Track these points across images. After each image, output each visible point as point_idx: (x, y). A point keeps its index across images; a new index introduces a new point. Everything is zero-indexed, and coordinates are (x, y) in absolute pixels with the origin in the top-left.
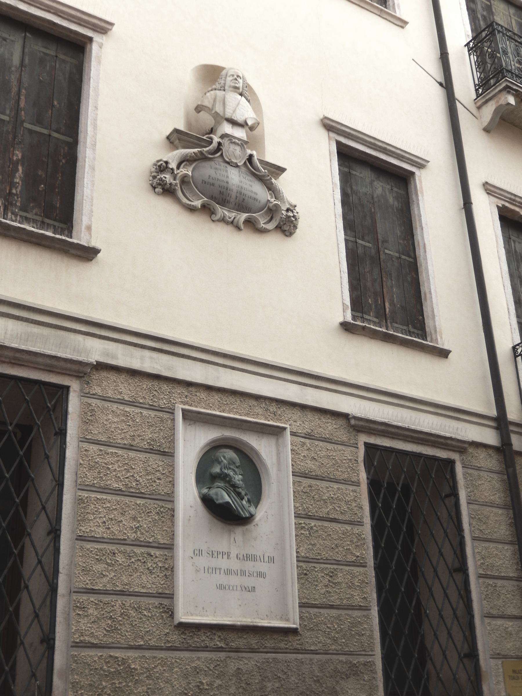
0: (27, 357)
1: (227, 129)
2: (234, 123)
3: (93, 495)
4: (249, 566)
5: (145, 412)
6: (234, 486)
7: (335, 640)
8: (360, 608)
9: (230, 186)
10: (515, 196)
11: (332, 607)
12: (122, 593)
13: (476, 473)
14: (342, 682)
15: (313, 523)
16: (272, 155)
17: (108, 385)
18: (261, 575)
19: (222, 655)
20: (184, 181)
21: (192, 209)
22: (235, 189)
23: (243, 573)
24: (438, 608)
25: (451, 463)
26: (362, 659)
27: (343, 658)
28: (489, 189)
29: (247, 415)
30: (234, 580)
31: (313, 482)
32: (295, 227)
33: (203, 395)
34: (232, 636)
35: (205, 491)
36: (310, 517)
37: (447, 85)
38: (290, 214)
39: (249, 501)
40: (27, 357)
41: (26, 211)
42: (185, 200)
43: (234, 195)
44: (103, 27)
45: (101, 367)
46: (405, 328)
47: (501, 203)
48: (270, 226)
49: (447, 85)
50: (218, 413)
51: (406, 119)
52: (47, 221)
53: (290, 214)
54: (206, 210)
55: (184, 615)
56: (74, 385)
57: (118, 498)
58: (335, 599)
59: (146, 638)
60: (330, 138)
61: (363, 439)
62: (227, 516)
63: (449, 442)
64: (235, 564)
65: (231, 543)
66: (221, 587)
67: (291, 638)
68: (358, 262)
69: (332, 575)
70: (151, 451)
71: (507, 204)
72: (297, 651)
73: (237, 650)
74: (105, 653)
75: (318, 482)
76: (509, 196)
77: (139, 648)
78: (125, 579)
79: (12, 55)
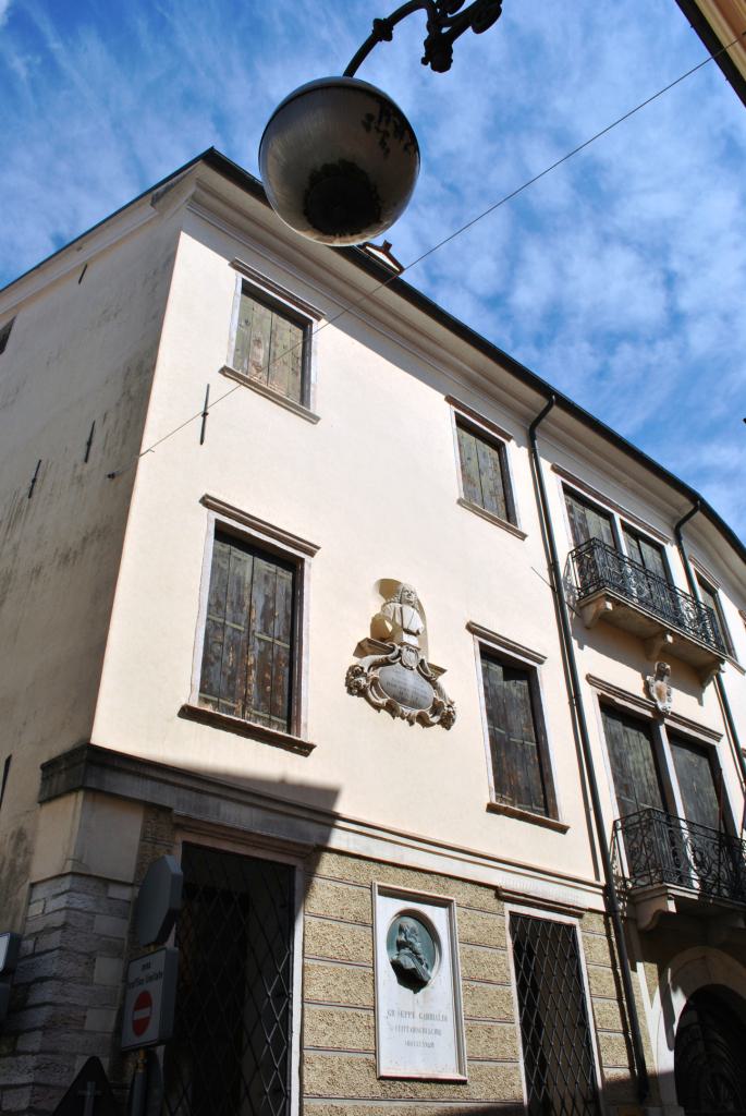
0: (265, 841)
1: (406, 638)
2: (409, 632)
3: (316, 963)
4: (429, 1024)
5: (350, 888)
6: (416, 953)
9: (408, 687)
11: (491, 1060)
12: (339, 1050)
15: (475, 984)
16: (433, 658)
18: (437, 1032)
20: (374, 682)
21: (377, 707)
22: (411, 689)
23: (424, 1031)
24: (250, 1098)
25: (292, 868)
28: (591, 679)
29: (423, 888)
30: (419, 1037)
31: (474, 948)
32: (454, 721)
33: (391, 870)
34: (418, 1086)
35: (395, 957)
38: (451, 709)
39: (427, 966)
40: (265, 841)
41: (258, 710)
42: (373, 699)
43: (410, 694)
44: (311, 550)
46: (529, 807)
50: (402, 888)
51: (533, 627)
52: (274, 718)
53: (451, 709)
54: (391, 709)
55: (384, 1072)
57: (334, 965)
58: (492, 1053)
59: (357, 1089)
61: (509, 907)
62: (412, 980)
64: (418, 1023)
66: (409, 1043)
68: (498, 745)
69: (489, 1030)
70: (356, 922)
71: (605, 693)
74: (328, 1103)
77: (352, 1098)
78: (340, 1037)
79: (244, 573)
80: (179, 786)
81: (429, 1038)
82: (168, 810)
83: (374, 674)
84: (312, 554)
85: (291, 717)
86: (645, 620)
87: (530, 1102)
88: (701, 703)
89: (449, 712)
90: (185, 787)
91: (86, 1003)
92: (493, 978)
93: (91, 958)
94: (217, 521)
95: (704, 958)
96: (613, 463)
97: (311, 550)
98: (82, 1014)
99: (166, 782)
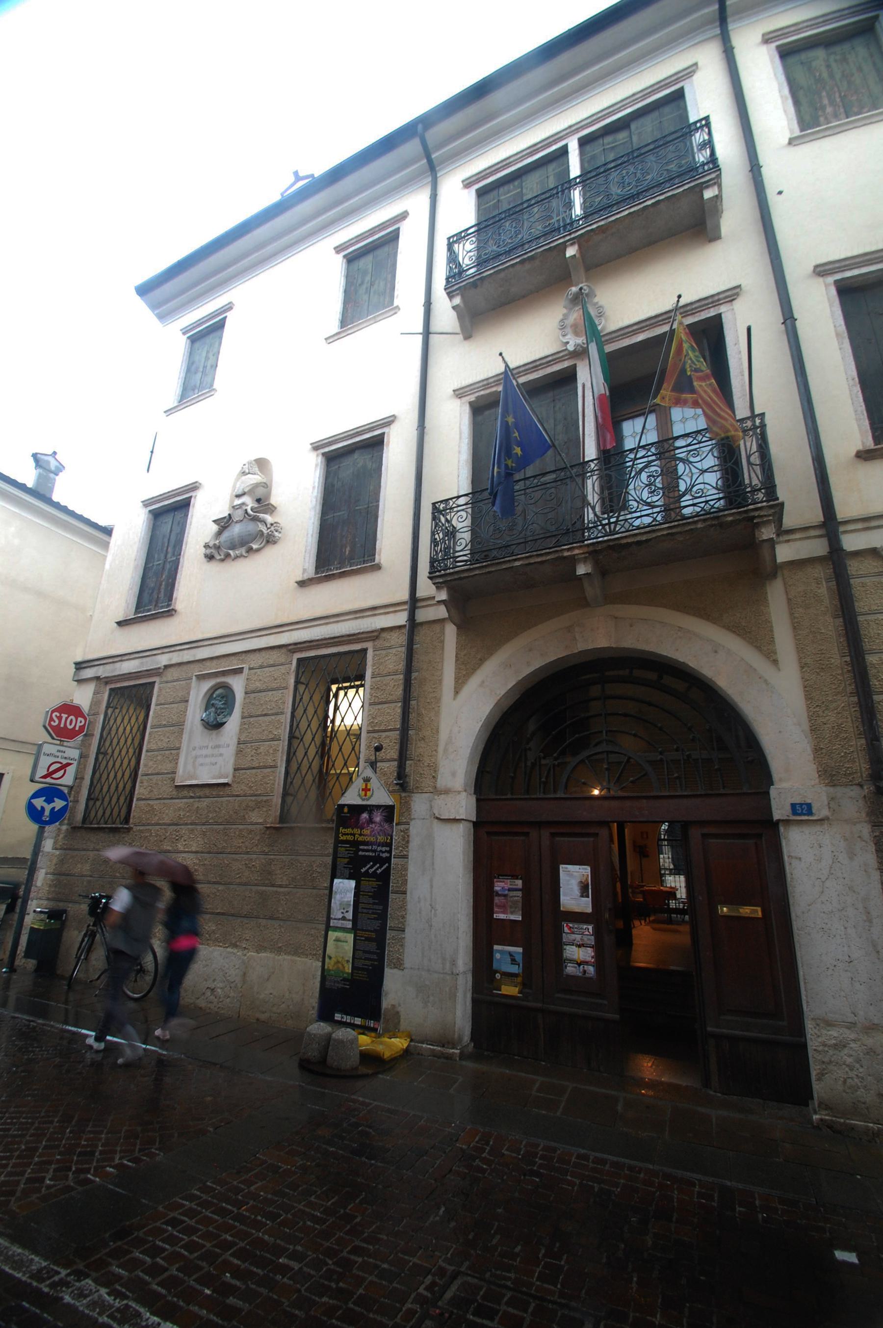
7: (251, 787)
8: (271, 767)
10: (487, 379)
11: (254, 768)
12: (158, 774)
13: (384, 652)
14: (250, 813)
17: (171, 674)
18: (221, 755)
19: (192, 800)
23: (213, 755)
26: (265, 798)
27: (253, 798)
34: (197, 790)
36: (252, 717)
45: (166, 667)
56: (369, 645)
63: (359, 636)
65: (211, 739)
67: (227, 788)
72: (229, 796)
73: (200, 797)
75: (260, 694)
76: (481, 384)
77: (160, 799)
86: (527, 266)
88: (169, 412)
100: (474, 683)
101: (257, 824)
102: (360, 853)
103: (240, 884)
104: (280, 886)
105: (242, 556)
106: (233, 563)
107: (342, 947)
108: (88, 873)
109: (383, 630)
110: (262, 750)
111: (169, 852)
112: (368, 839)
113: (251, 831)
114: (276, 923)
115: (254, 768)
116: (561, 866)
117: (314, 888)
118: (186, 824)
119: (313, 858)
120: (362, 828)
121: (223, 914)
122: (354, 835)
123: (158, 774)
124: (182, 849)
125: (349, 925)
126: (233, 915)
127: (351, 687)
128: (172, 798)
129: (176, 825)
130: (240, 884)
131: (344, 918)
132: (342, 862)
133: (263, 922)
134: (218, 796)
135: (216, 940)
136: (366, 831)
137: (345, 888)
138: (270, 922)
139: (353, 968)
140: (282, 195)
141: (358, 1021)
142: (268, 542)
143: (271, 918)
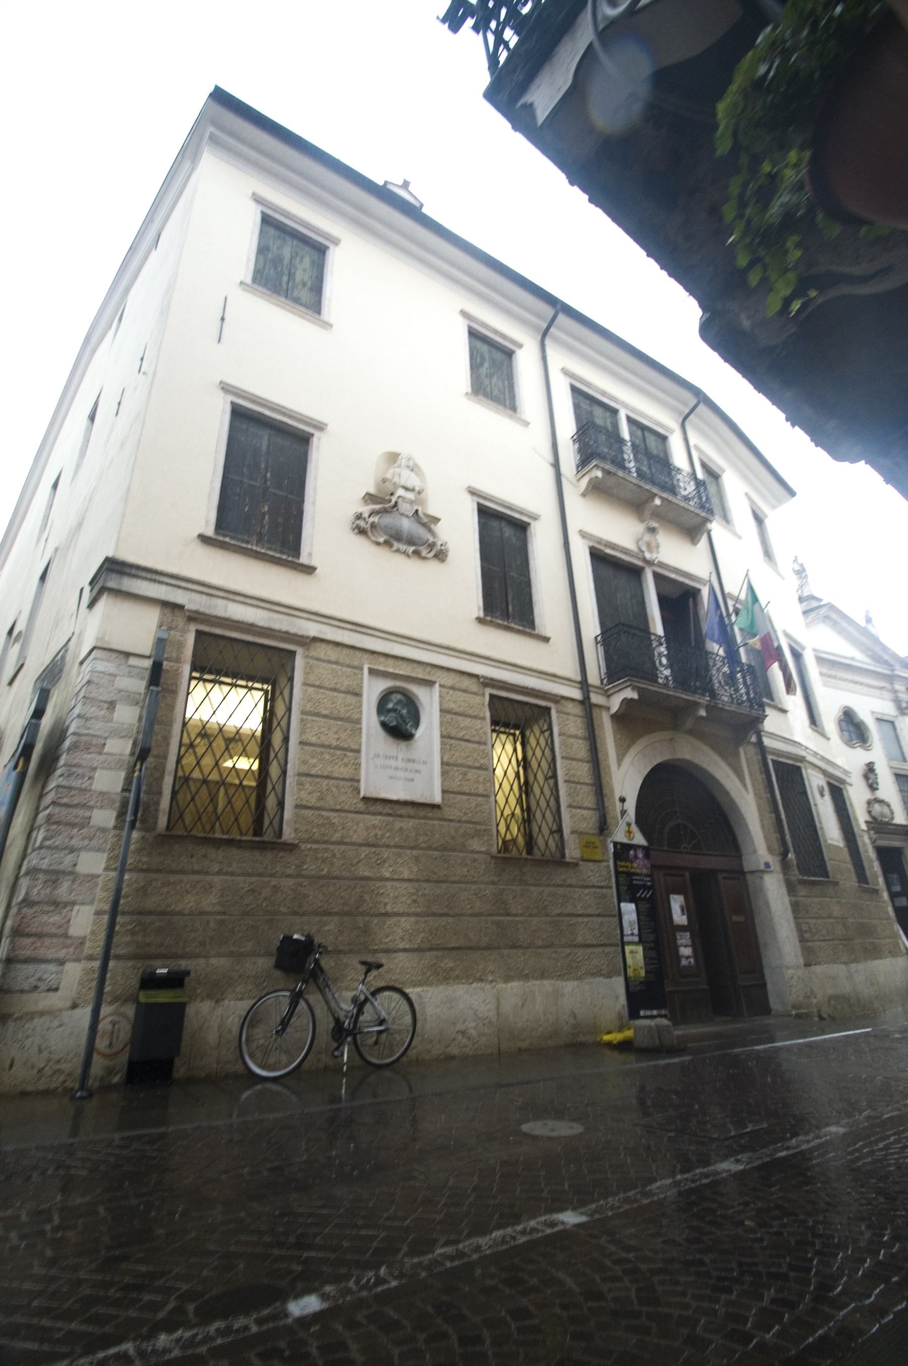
4: (410, 766)
11: (464, 794)
12: (327, 777)
17: (322, 651)
18: (417, 771)
19: (391, 819)
20: (373, 526)
23: (406, 770)
26: (483, 827)
28: (583, 535)
30: (401, 774)
31: (454, 717)
33: (382, 659)
37: (556, 465)
44: (535, 518)
47: (591, 544)
48: (431, 555)
49: (556, 465)
51: (525, 489)
58: (466, 789)
60: (473, 500)
61: (488, 691)
64: (400, 764)
66: (391, 777)
67: (435, 810)
72: (440, 819)
73: (401, 816)
80: (192, 590)
81: (411, 776)
82: (181, 607)
83: (375, 519)
84: (806, 624)
85: (294, 546)
86: (634, 488)
87: (501, 8)
88: (867, 612)
89: (441, 550)
90: (196, 591)
91: (106, 735)
92: (472, 739)
93: (112, 705)
94: (232, 403)
95: (671, 739)
96: (618, 363)
97: (535, 518)
98: (103, 742)
99: (179, 587)
100: (627, 760)
101: (479, 852)
102: (634, 882)
103: (471, 915)
104: (516, 915)
105: (404, 553)
106: (392, 554)
107: (636, 956)
108: (218, 908)
109: (563, 698)
110: (470, 776)
111: (367, 879)
112: (638, 871)
113: (475, 860)
114: (520, 951)
115: (464, 794)
116: (671, 896)
117: (547, 915)
118: (388, 846)
119: (541, 889)
120: (632, 863)
121: (459, 948)
122: (627, 867)
123: (327, 777)
124: (388, 875)
125: (636, 939)
126: (470, 948)
127: (504, 733)
128: (357, 812)
129: (373, 846)
130: (471, 915)
131: (632, 934)
132: (624, 889)
133: (506, 952)
134: (425, 818)
135: (457, 977)
136: (635, 865)
137: (629, 910)
138: (512, 951)
139: (647, 972)
140: (386, 183)
141: (655, 1012)
142: (436, 556)
143: (513, 947)
